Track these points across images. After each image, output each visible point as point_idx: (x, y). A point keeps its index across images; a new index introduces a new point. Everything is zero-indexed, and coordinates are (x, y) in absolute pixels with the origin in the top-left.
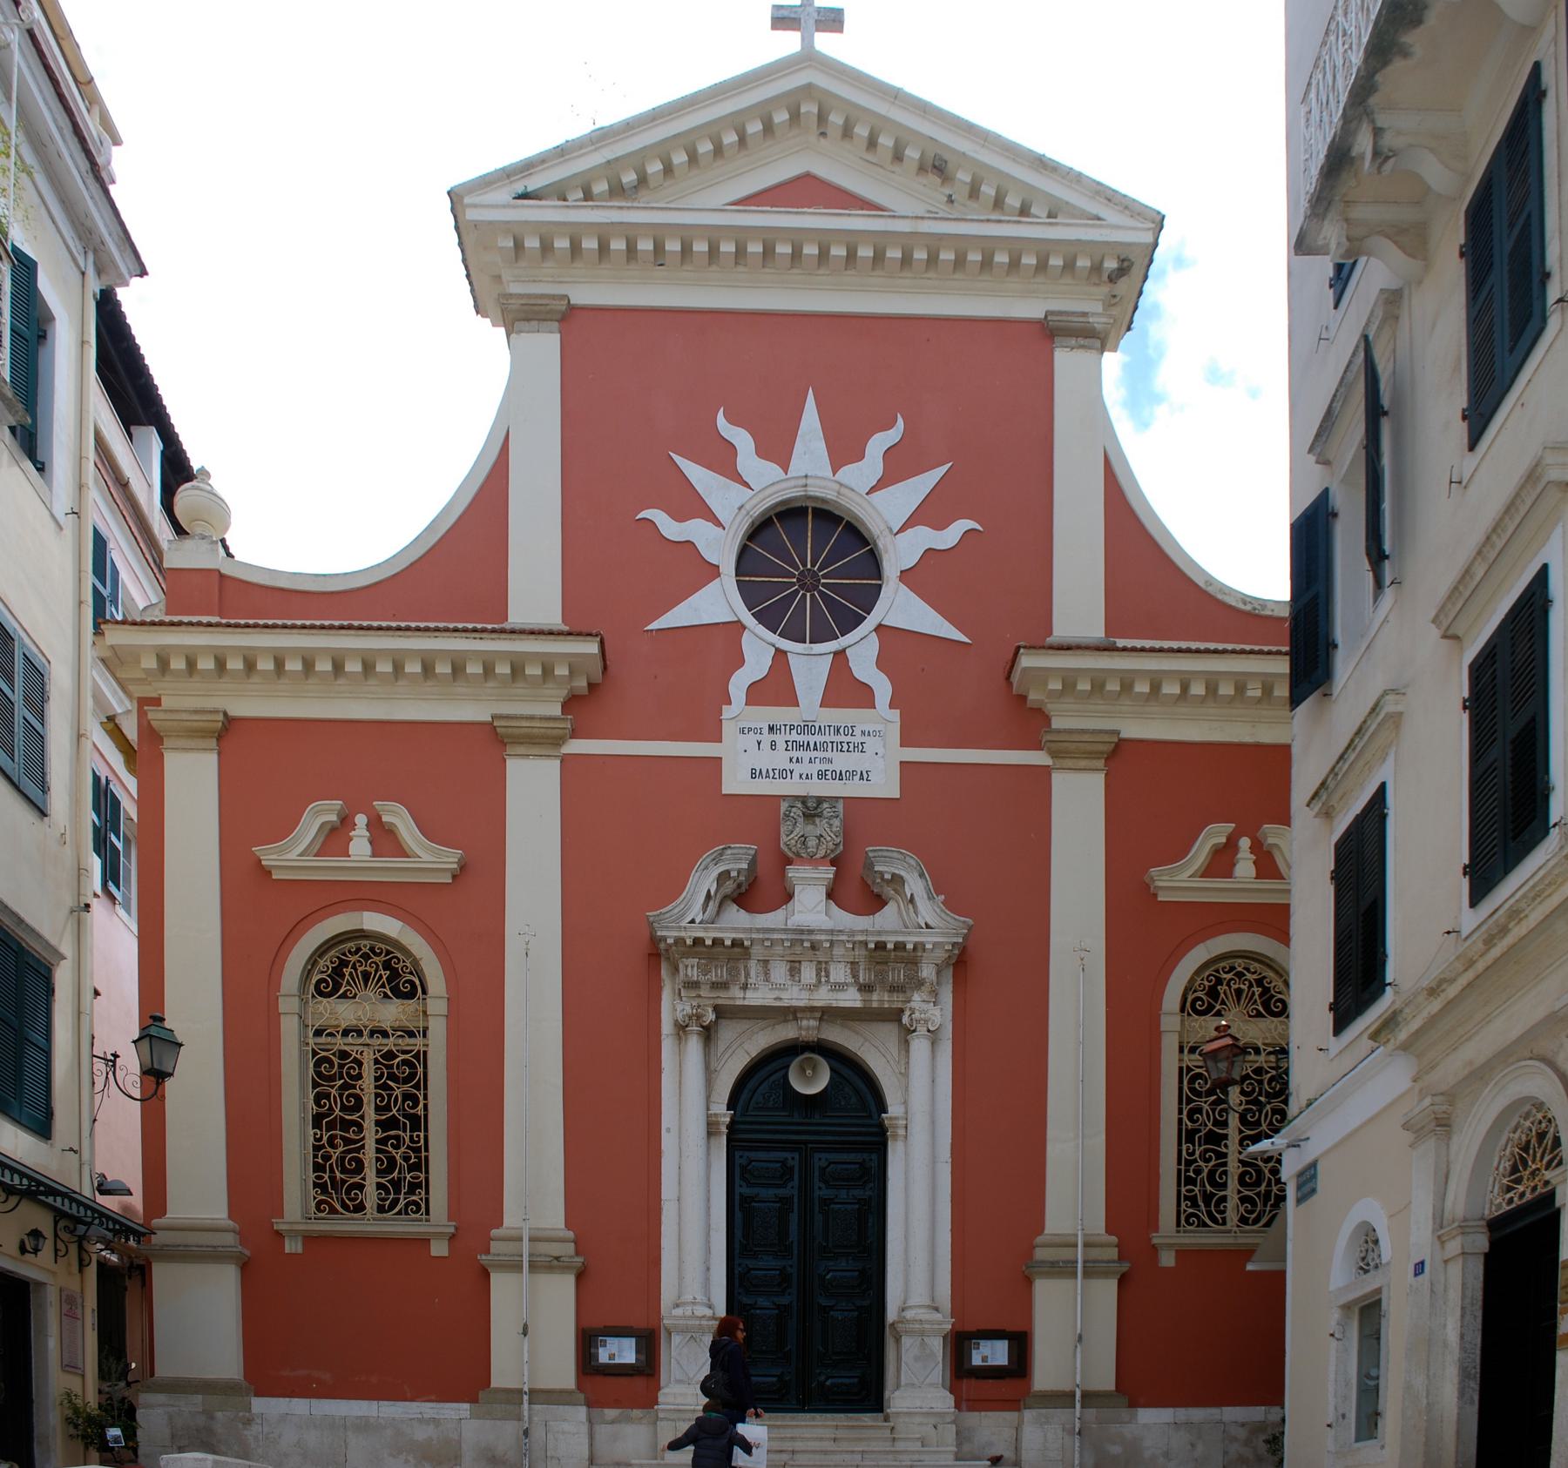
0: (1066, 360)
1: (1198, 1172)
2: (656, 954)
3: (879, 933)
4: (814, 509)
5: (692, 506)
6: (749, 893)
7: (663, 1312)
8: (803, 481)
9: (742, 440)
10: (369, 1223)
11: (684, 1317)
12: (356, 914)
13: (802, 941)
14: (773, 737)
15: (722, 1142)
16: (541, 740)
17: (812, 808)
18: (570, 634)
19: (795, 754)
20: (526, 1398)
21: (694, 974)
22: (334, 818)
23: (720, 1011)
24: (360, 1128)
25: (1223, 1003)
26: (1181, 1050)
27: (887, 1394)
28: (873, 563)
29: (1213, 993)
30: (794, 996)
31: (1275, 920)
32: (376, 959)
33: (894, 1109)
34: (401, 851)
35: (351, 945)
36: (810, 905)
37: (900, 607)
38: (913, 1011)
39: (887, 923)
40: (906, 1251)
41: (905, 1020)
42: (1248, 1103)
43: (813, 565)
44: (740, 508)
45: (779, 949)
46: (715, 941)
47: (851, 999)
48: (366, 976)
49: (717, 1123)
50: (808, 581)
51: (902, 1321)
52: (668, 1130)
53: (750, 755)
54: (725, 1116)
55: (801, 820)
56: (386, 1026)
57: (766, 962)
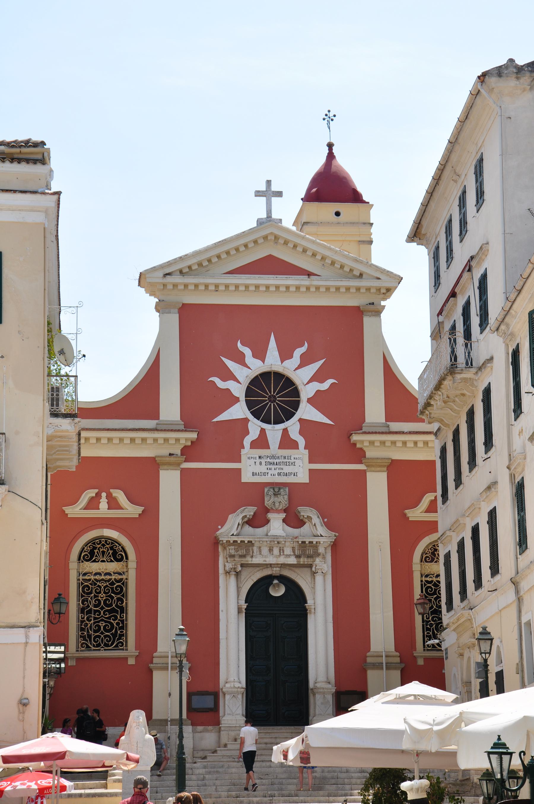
0: (367, 321)
5: (229, 376)
7: (221, 687)
9: (247, 352)
11: (231, 688)
12: (101, 530)
13: (274, 541)
16: (170, 462)
17: (276, 487)
19: (269, 467)
20: (169, 723)
21: (233, 552)
22: (94, 495)
26: (422, 576)
28: (296, 393)
30: (271, 560)
32: (107, 546)
33: (310, 602)
34: (119, 507)
36: (276, 526)
37: (307, 412)
40: (316, 658)
41: (313, 569)
43: (274, 393)
45: (265, 543)
47: (293, 560)
48: (103, 552)
50: (272, 399)
51: (316, 688)
52: (222, 611)
53: (252, 468)
54: (245, 606)
55: (273, 496)
57: (260, 547)
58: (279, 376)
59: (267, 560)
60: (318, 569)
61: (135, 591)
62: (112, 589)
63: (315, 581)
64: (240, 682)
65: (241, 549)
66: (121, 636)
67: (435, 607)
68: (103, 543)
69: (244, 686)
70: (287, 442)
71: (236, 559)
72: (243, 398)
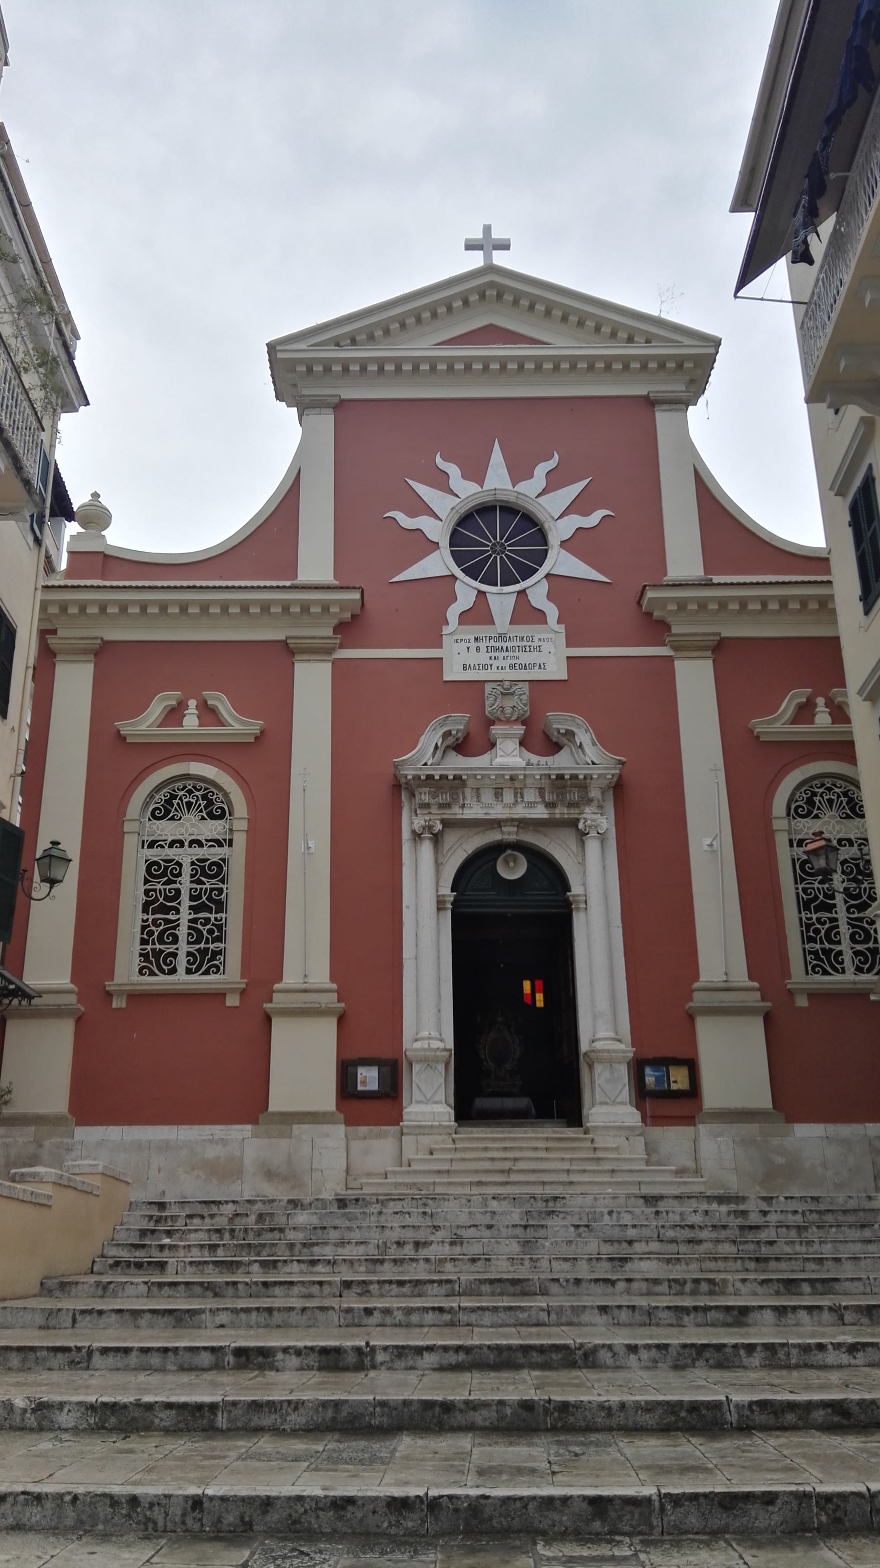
0: (663, 418)
1: (817, 931)
2: (399, 787)
3: (559, 769)
4: (500, 507)
5: (423, 508)
6: (462, 746)
8: (493, 492)
9: (453, 470)
10: (182, 979)
11: (423, 1050)
12: (186, 763)
14: (477, 644)
15: (447, 917)
17: (507, 690)
18: (342, 588)
19: (493, 654)
21: (426, 798)
23: (447, 824)
24: (178, 912)
25: (819, 809)
26: (791, 845)
27: (585, 1112)
28: (542, 537)
29: (810, 802)
30: (498, 812)
31: (845, 750)
32: (197, 793)
33: (576, 889)
35: (180, 785)
36: (508, 755)
37: (560, 562)
38: (586, 820)
39: (562, 762)
41: (581, 826)
42: (849, 880)
44: (452, 509)
45: (487, 781)
46: (441, 776)
47: (540, 812)
49: (444, 902)
52: (408, 907)
53: (461, 656)
56: (202, 838)
57: (478, 789)
58: (509, 510)
59: (491, 811)
60: (590, 827)
61: (244, 871)
62: (202, 868)
63: (584, 856)
64: (441, 1040)
65: (442, 794)
66: (216, 953)
67: (821, 897)
68: (190, 787)
69: (450, 1045)
70: (526, 614)
71: (433, 811)
72: (445, 543)
